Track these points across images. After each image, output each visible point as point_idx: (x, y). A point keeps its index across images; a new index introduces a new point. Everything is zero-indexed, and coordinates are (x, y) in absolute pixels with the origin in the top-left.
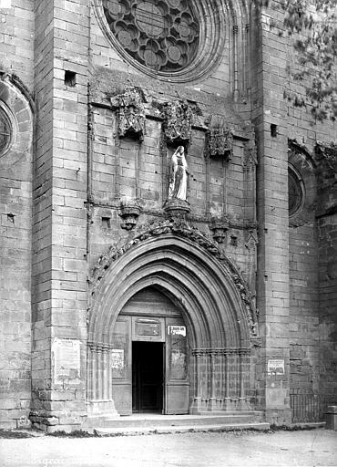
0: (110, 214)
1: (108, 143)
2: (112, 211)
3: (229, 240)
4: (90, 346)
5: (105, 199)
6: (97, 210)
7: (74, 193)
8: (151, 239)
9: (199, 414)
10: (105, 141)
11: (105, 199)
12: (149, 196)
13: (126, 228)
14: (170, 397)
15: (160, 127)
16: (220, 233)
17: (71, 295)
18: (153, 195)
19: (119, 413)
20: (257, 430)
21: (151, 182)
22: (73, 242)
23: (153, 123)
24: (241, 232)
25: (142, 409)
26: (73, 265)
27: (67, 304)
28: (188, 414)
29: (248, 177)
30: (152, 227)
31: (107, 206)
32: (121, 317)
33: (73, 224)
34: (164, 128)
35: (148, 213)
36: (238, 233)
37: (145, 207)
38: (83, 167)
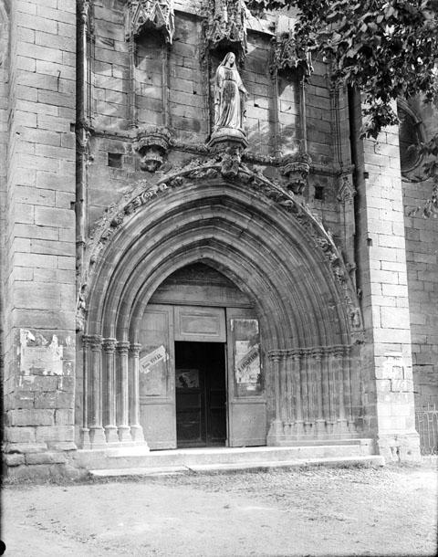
0: (122, 148)
1: (117, 49)
2: (125, 145)
3: (312, 191)
4: (84, 341)
5: (114, 127)
6: (99, 142)
7: (54, 110)
8: (190, 186)
9: (279, 445)
10: (113, 45)
11: (113, 126)
12: (184, 125)
13: (145, 169)
14: (239, 419)
15: (199, 29)
16: (295, 178)
17: (49, 262)
18: (191, 124)
19: (148, 445)
20: (152, 478)
21: (187, 105)
22: (52, 186)
23: (188, 25)
24: (330, 180)
25: (213, 441)
26: (53, 217)
27: (40, 276)
28: (265, 446)
29: (337, 104)
30: (188, 168)
31: (115, 136)
32: (151, 307)
33: (52, 156)
34: (205, 29)
35: (184, 149)
36: (325, 181)
37: (178, 141)
38: (69, 73)
